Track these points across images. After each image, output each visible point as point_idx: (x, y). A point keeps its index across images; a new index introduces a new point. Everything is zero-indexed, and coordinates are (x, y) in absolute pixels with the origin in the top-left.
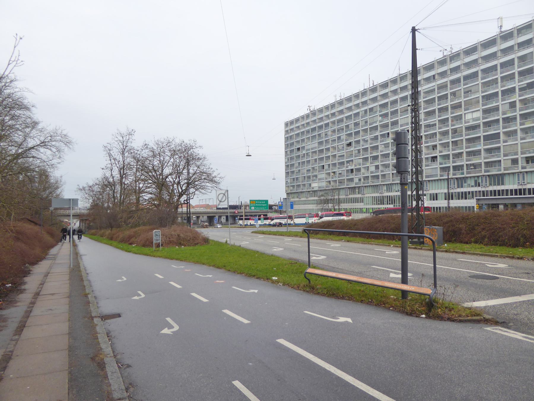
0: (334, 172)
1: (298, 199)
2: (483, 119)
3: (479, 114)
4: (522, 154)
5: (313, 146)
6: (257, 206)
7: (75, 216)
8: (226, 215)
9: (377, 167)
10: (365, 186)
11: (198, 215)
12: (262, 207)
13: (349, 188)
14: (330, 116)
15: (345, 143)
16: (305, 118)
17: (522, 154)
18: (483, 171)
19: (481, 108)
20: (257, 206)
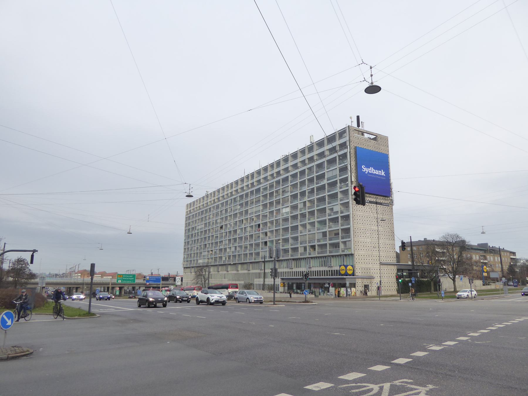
0: (212, 251)
1: (246, 272)
2: (291, 213)
3: (288, 210)
4: (309, 243)
5: (257, 209)
6: (124, 280)
7: (471, 255)
8: (108, 286)
9: (324, 234)
10: (333, 256)
11: (134, 286)
12: (129, 280)
13: (293, 259)
14: (307, 162)
15: (219, 225)
16: (275, 166)
17: (309, 243)
18: (328, 252)
19: (289, 204)
20: (124, 280)
